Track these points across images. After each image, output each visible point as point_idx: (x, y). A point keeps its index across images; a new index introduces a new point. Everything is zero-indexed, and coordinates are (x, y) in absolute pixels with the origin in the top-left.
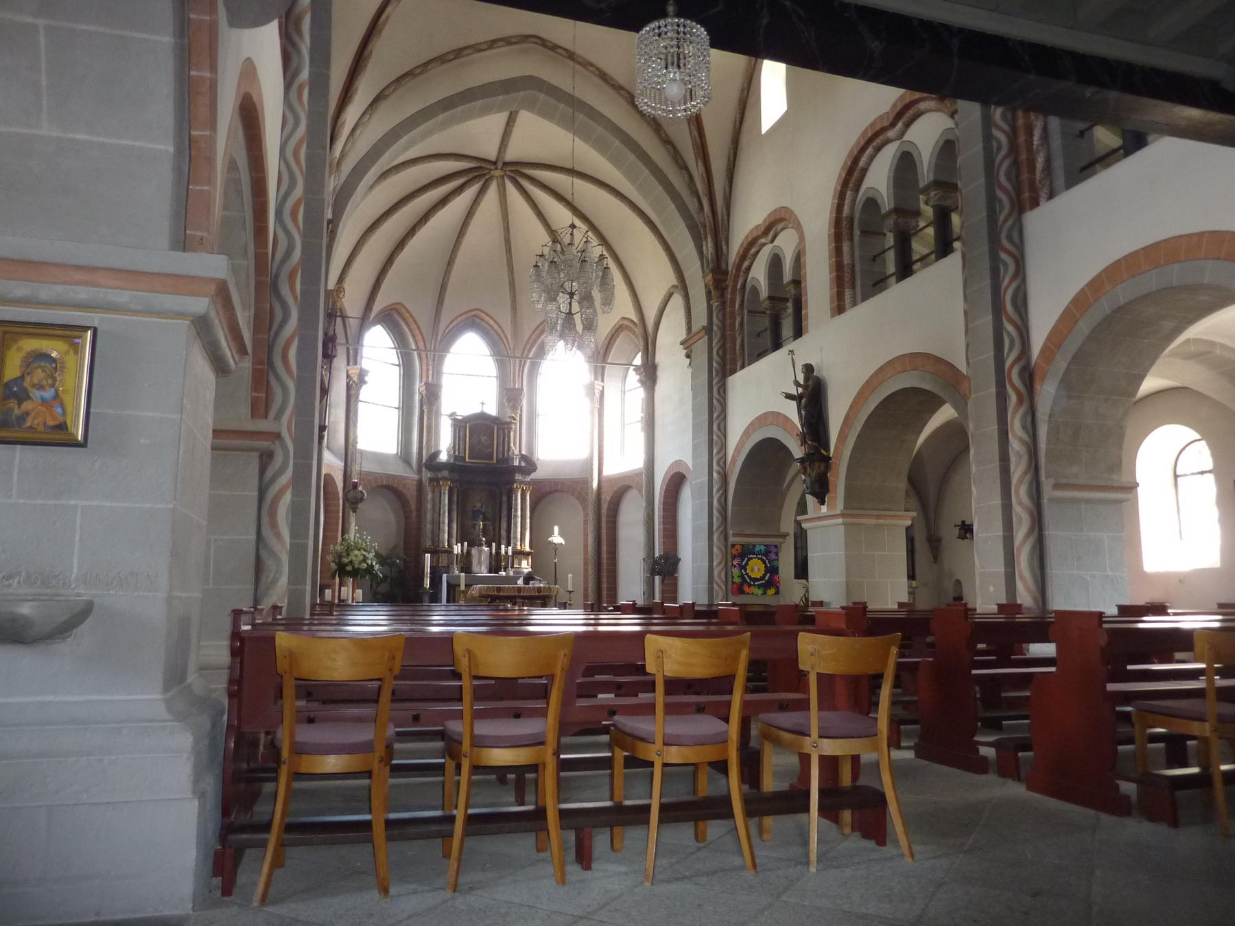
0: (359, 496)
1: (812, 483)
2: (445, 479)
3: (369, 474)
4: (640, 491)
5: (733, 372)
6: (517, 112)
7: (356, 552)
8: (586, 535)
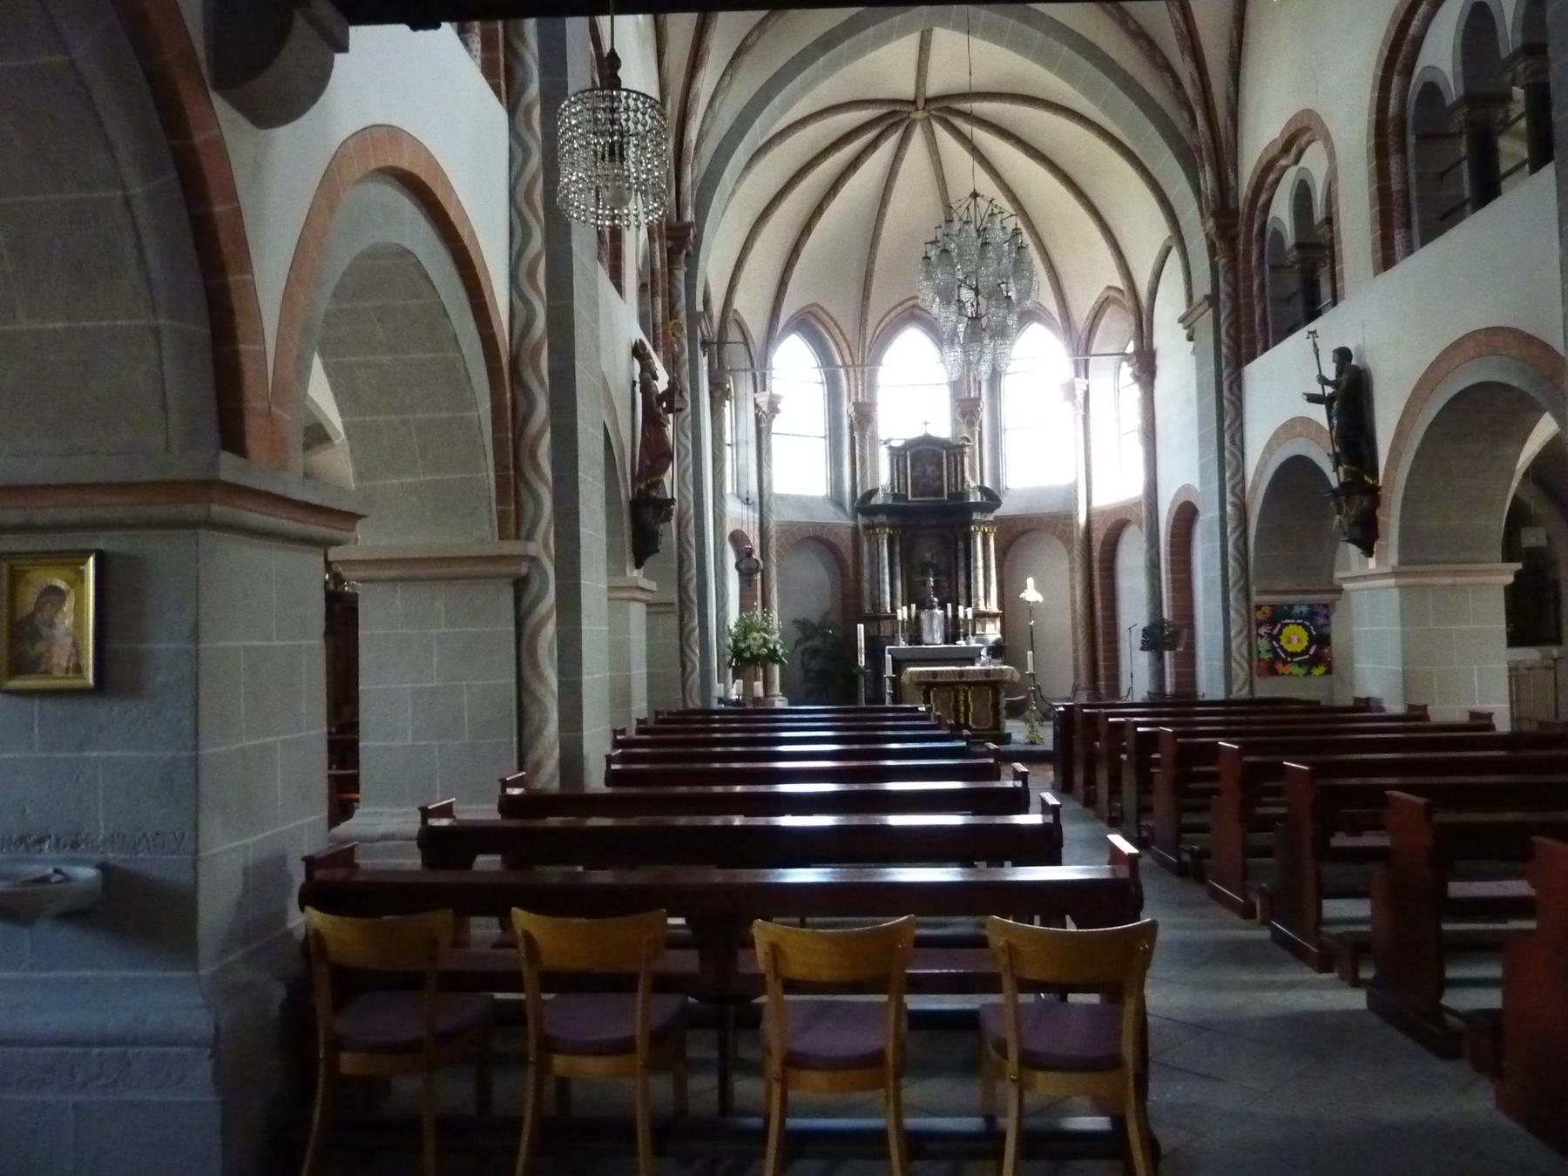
0: (754, 565)
1: (1352, 526)
2: (882, 525)
3: (792, 524)
4: (1140, 527)
5: (1252, 357)
6: (930, 31)
7: (755, 635)
8: (1072, 587)
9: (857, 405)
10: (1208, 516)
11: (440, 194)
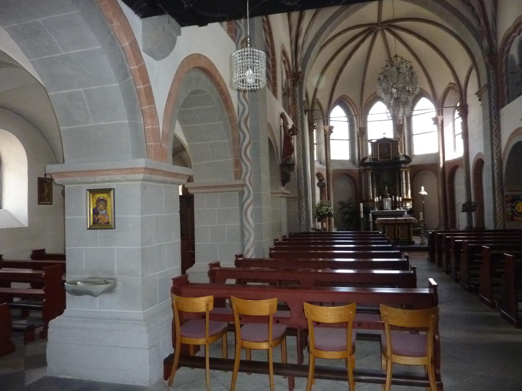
2: (369, 169)
3: (337, 170)
4: (463, 168)
5: (503, 106)
7: (324, 207)
8: (438, 189)
9: (360, 128)
10: (488, 163)
11: (214, 73)
